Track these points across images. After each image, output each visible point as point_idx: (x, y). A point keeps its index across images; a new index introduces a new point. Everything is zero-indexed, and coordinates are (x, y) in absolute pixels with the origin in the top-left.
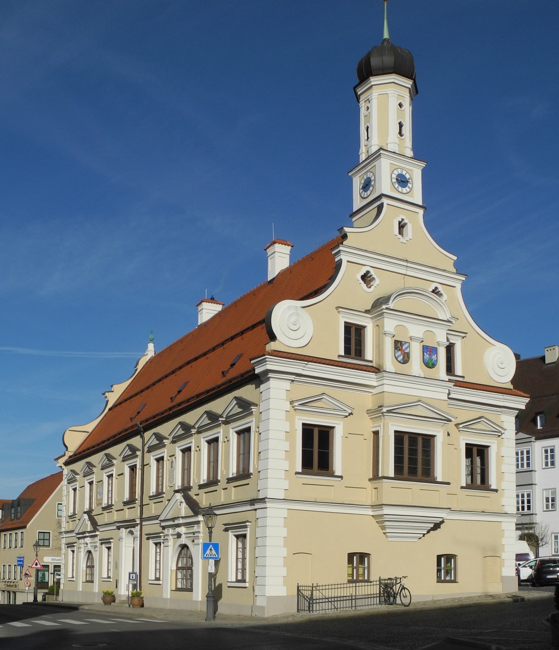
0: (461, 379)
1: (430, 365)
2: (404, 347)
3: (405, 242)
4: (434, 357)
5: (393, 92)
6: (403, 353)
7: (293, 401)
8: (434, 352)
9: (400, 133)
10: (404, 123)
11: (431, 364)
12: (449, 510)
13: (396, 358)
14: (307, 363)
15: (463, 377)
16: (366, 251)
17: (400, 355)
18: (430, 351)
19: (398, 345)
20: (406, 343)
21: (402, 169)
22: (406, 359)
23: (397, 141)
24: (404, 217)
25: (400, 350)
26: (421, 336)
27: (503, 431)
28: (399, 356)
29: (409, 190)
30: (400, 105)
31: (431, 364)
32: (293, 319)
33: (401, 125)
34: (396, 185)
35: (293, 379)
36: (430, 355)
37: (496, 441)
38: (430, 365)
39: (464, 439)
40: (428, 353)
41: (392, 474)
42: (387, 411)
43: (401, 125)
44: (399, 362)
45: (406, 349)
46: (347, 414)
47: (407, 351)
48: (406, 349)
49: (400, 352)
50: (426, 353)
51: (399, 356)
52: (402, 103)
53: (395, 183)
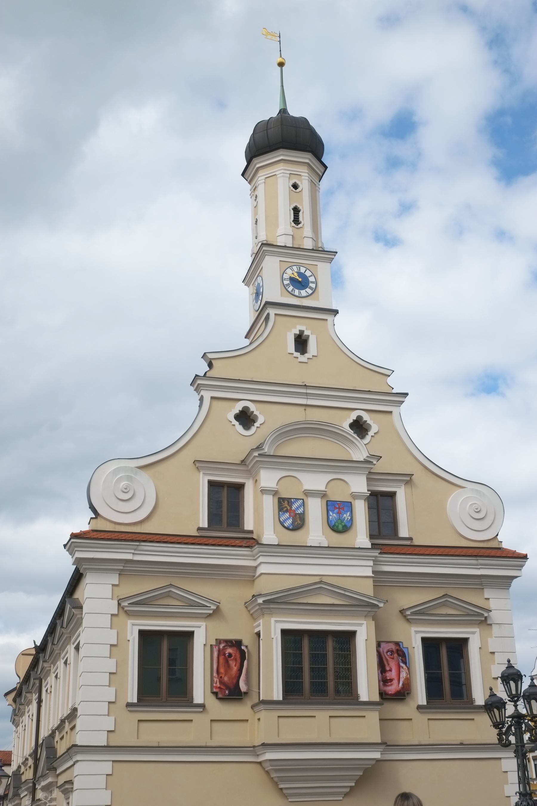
0: (408, 543)
1: (341, 528)
2: (294, 507)
3: (306, 360)
4: (347, 516)
5: (282, 175)
6: (292, 514)
7: (403, 610)
8: (345, 509)
9: (296, 221)
10: (301, 208)
11: (340, 527)
12: (388, 744)
13: (282, 524)
14: (138, 544)
15: (411, 539)
16: (239, 381)
17: (288, 519)
18: (339, 508)
19: (284, 504)
20: (297, 499)
21: (299, 265)
22: (299, 523)
23: (290, 231)
24: (303, 328)
25: (287, 511)
26: (323, 488)
27: (486, 615)
28: (285, 520)
29: (310, 291)
30: (295, 186)
31: (340, 527)
32: (123, 484)
33: (296, 211)
34: (290, 288)
35: (122, 568)
36: (339, 513)
37: (365, 622)
38: (341, 528)
39: (417, 632)
40: (336, 511)
41: (277, 694)
42: (264, 601)
43: (296, 211)
44: (287, 528)
45: (298, 508)
46: (211, 612)
47: (300, 511)
48: (298, 508)
49: (287, 515)
50: (332, 511)
51: (285, 520)
52: (298, 182)
53: (288, 285)
